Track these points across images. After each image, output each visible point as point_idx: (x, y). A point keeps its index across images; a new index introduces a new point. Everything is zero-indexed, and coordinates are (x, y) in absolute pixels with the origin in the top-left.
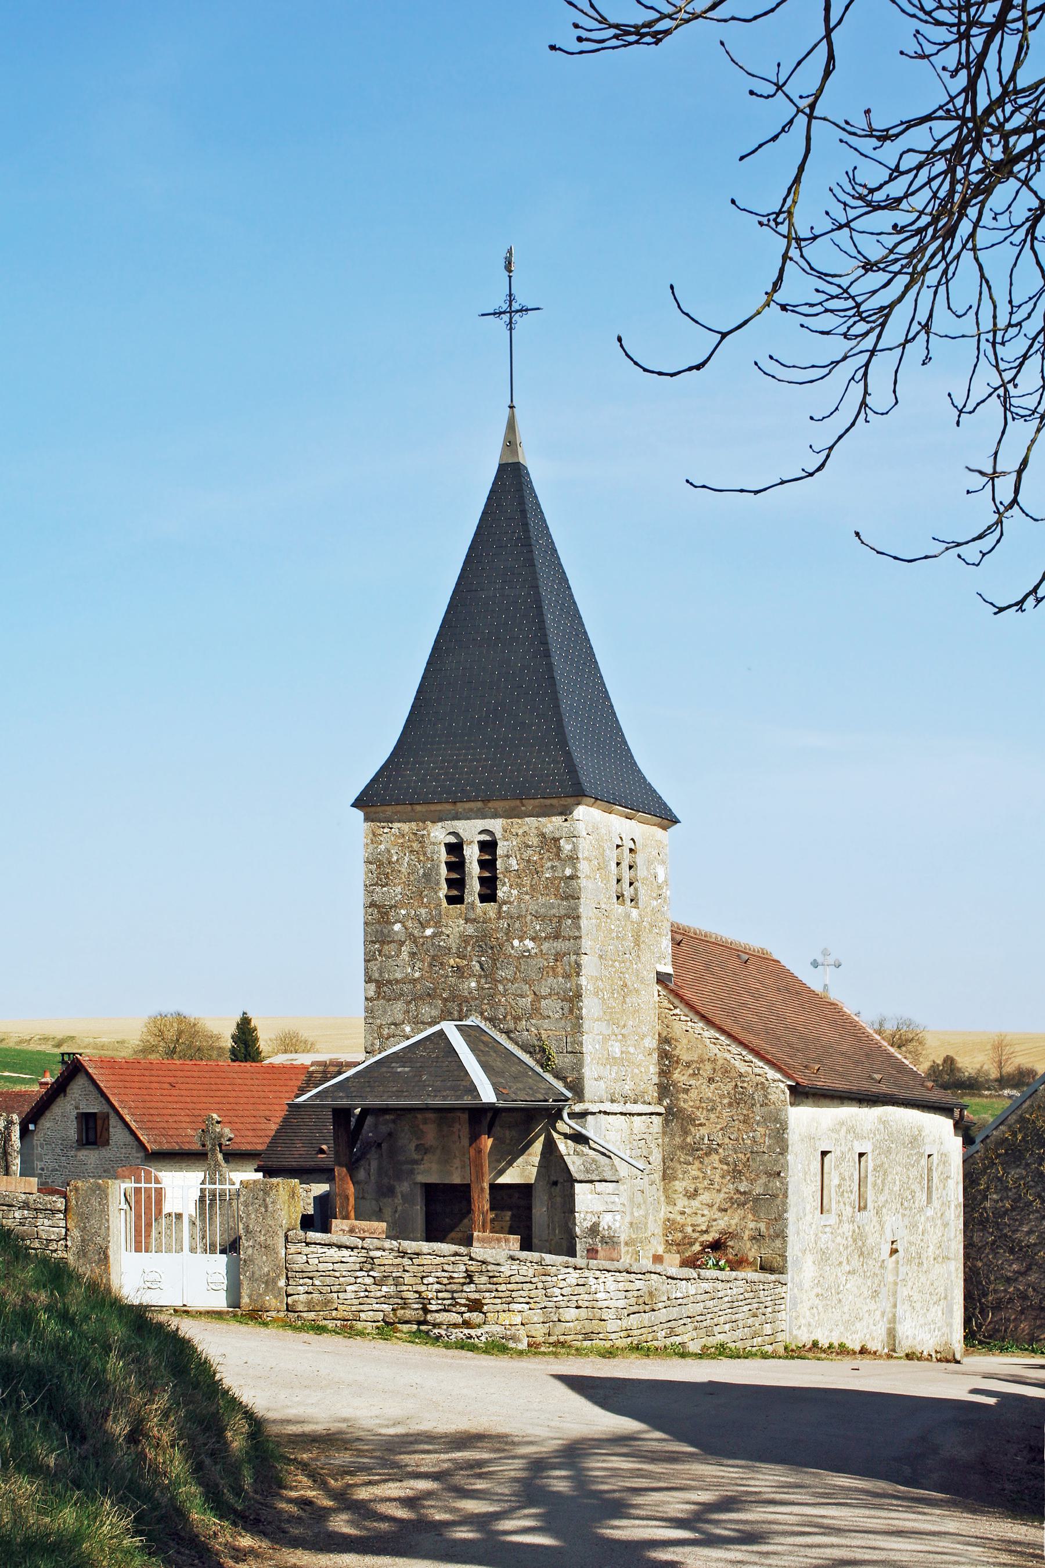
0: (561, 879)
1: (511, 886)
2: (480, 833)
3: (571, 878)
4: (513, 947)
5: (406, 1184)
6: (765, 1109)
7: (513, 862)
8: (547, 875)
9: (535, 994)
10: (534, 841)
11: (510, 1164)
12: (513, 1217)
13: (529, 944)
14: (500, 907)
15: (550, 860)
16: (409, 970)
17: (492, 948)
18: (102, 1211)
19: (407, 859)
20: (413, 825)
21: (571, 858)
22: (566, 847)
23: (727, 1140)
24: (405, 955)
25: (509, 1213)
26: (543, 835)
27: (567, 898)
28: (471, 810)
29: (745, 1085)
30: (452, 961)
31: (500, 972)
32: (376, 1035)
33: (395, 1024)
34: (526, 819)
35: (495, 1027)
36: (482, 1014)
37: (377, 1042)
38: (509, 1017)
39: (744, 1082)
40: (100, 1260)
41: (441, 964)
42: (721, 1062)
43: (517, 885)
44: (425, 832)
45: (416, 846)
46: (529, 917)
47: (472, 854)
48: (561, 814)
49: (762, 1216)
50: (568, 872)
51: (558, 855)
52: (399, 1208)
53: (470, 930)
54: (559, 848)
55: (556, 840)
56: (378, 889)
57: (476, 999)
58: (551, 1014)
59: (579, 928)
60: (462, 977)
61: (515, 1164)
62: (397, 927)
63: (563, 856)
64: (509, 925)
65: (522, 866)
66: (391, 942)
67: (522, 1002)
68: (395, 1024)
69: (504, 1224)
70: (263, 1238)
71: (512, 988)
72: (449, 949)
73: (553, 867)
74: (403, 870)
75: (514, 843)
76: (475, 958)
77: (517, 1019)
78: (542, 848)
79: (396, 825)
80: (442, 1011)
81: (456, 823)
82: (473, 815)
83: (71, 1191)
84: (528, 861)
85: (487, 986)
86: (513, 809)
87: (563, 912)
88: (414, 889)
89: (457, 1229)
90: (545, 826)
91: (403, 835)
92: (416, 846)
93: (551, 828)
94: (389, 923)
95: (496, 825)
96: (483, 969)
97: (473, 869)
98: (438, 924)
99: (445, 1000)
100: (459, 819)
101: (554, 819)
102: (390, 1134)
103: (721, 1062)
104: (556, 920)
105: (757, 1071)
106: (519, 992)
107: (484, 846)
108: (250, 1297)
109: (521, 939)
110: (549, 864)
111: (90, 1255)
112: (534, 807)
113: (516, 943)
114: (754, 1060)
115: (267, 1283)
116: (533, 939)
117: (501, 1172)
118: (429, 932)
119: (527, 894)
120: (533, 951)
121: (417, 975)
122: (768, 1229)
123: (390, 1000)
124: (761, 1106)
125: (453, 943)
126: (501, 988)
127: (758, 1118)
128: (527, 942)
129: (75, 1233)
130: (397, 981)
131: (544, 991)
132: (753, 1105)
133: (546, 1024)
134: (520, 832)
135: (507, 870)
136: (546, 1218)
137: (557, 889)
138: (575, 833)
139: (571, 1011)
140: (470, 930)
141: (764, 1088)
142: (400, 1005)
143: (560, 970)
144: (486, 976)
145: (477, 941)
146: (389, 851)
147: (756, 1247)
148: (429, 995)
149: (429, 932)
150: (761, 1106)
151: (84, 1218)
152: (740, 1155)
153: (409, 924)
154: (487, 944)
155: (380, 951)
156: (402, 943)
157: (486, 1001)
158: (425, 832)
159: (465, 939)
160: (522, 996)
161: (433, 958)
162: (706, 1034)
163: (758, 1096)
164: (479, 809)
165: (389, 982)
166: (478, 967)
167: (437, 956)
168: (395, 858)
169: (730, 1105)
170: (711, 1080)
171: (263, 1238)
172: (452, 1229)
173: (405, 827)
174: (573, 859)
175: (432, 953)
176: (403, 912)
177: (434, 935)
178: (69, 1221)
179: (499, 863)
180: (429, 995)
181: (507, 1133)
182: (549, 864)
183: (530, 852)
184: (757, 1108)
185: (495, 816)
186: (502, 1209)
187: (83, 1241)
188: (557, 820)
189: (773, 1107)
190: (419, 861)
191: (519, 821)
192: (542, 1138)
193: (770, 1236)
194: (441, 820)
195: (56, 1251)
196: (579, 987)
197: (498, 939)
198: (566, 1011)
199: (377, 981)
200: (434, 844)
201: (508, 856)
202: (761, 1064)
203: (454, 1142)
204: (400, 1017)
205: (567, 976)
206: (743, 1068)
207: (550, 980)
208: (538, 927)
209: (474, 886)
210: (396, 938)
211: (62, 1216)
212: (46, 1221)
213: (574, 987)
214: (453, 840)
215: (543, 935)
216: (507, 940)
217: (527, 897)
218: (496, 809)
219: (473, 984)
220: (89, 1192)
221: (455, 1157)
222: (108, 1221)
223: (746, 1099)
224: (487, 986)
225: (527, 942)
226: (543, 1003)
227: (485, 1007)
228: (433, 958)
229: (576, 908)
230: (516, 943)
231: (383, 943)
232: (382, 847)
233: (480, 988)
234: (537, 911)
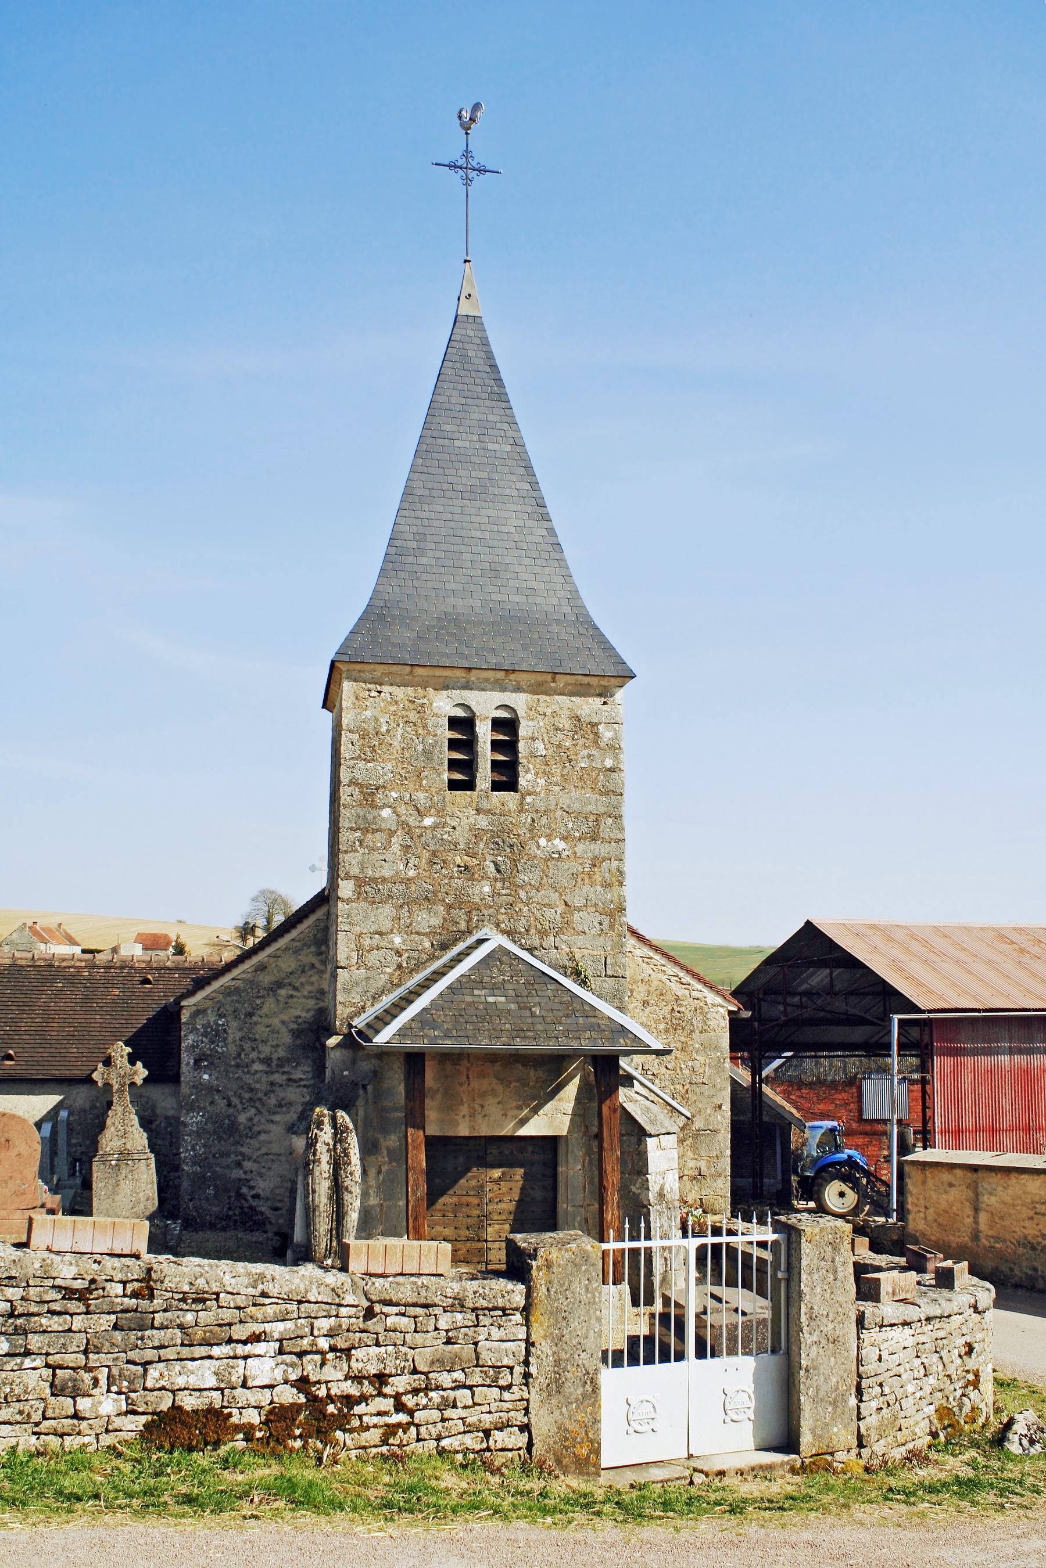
0: (600, 770)
1: (537, 774)
2: (497, 708)
3: (612, 770)
4: (538, 847)
5: (393, 1137)
6: (704, 1036)
7: (540, 745)
8: (583, 765)
9: (566, 904)
10: (566, 723)
11: (535, 1111)
12: (526, 1177)
13: (559, 844)
14: (523, 798)
15: (586, 747)
16: (401, 867)
17: (511, 846)
18: (592, 1303)
19: (400, 731)
20: (410, 690)
21: (611, 747)
22: (606, 734)
23: (663, 1070)
24: (396, 848)
25: (521, 1171)
26: (578, 718)
27: (607, 794)
28: (487, 680)
29: (682, 1009)
30: (458, 861)
31: (522, 876)
32: (353, 946)
33: (381, 934)
34: (557, 697)
35: (515, 942)
36: (497, 925)
37: (354, 955)
38: (533, 931)
39: (681, 1005)
40: (584, 1396)
41: (444, 862)
42: (655, 984)
43: (544, 773)
44: (425, 701)
45: (413, 716)
46: (559, 813)
47: (484, 732)
48: (600, 695)
49: (703, 1153)
50: (609, 763)
51: (596, 742)
52: (384, 1169)
53: (483, 822)
54: (597, 734)
55: (594, 725)
56: (361, 764)
57: (491, 907)
58: (586, 929)
59: (622, 829)
60: (472, 879)
61: (541, 1112)
62: (386, 813)
63: (602, 744)
64: (533, 820)
65: (550, 751)
66: (377, 830)
67: (549, 913)
68: (381, 934)
69: (512, 1184)
70: (831, 1326)
71: (538, 896)
72: (456, 844)
73: (589, 756)
74: (396, 743)
75: (541, 724)
76: (489, 858)
77: (543, 933)
78: (576, 733)
79: (386, 689)
80: (445, 919)
81: (466, 693)
82: (489, 686)
83: (539, 1269)
84: (559, 746)
85: (504, 892)
86: (540, 684)
87: (602, 810)
88: (410, 768)
89: (451, 1192)
90: (580, 707)
91: (396, 702)
92: (413, 716)
93: (587, 711)
94: (373, 806)
95: (520, 701)
96: (499, 871)
97: (486, 755)
98: (441, 812)
99: (449, 907)
100: (471, 689)
101: (590, 700)
102: (375, 1073)
103: (655, 984)
104: (592, 818)
105: (695, 994)
106: (546, 901)
107: (498, 724)
108: (813, 1431)
109: (549, 838)
110: (585, 752)
111: (568, 1388)
112: (566, 684)
113: (543, 842)
114: (692, 982)
115: (834, 1403)
116: (564, 838)
117: (523, 1122)
118: (428, 821)
119: (557, 784)
120: (564, 854)
121: (411, 873)
122: (708, 1168)
123: (374, 902)
124: (701, 1032)
125: (462, 837)
126: (522, 894)
127: (697, 1046)
128: (557, 842)
129: (544, 1348)
130: (384, 880)
131: (578, 901)
132: (691, 1031)
133: (580, 941)
134: (549, 711)
135: (533, 755)
136: (581, 1179)
137: (595, 781)
138: (618, 720)
139: (612, 926)
140: (483, 822)
141: (704, 1014)
142: (387, 911)
143: (598, 877)
144: (503, 880)
145: (492, 837)
146: (376, 720)
147: (696, 1188)
148: (427, 899)
149: (428, 821)
150: (701, 1032)
151: (561, 1317)
152: (678, 1087)
153: (402, 809)
154: (507, 846)
155: (361, 842)
156: (392, 833)
157: (503, 910)
158: (425, 701)
159: (477, 834)
160: (550, 906)
161: (434, 853)
162: (638, 952)
163: (697, 1022)
164: (497, 680)
165: (374, 880)
166: (492, 868)
167: (438, 851)
168: (384, 729)
169: (667, 1030)
170: (645, 1003)
171: (831, 1326)
172: (449, 1189)
173: (400, 692)
174: (614, 748)
175: (432, 848)
176: (394, 795)
177: (435, 827)
178: (535, 1326)
179: (521, 746)
180: (427, 899)
181: (532, 1073)
182: (585, 752)
183: (560, 735)
184: (696, 1035)
185: (518, 689)
186: (511, 1165)
187: (557, 1362)
188: (596, 702)
189: (713, 1034)
190: (418, 735)
191: (547, 698)
192: (576, 1080)
193: (712, 1176)
194: (446, 688)
195: (509, 1387)
196: (622, 899)
197: (519, 835)
198: (606, 926)
199: (356, 878)
200: (435, 715)
201: (533, 739)
202: (700, 987)
203: (461, 1084)
204: (386, 925)
205: (607, 885)
206: (680, 991)
207: (586, 889)
208: (570, 825)
209: (484, 776)
210: (383, 826)
211: (518, 1317)
212: (494, 1330)
213: (616, 899)
214: (460, 713)
215: (577, 834)
216: (532, 838)
217: (557, 788)
218: (518, 682)
219: (487, 889)
220: (570, 1268)
221: (462, 1102)
222: (599, 1320)
223: (684, 1024)
224: (504, 892)
225: (557, 842)
226: (577, 916)
227: (501, 917)
228: (434, 853)
229: (616, 807)
230: (543, 842)
231: (365, 831)
232: (368, 713)
233: (494, 894)
234: (569, 807)
